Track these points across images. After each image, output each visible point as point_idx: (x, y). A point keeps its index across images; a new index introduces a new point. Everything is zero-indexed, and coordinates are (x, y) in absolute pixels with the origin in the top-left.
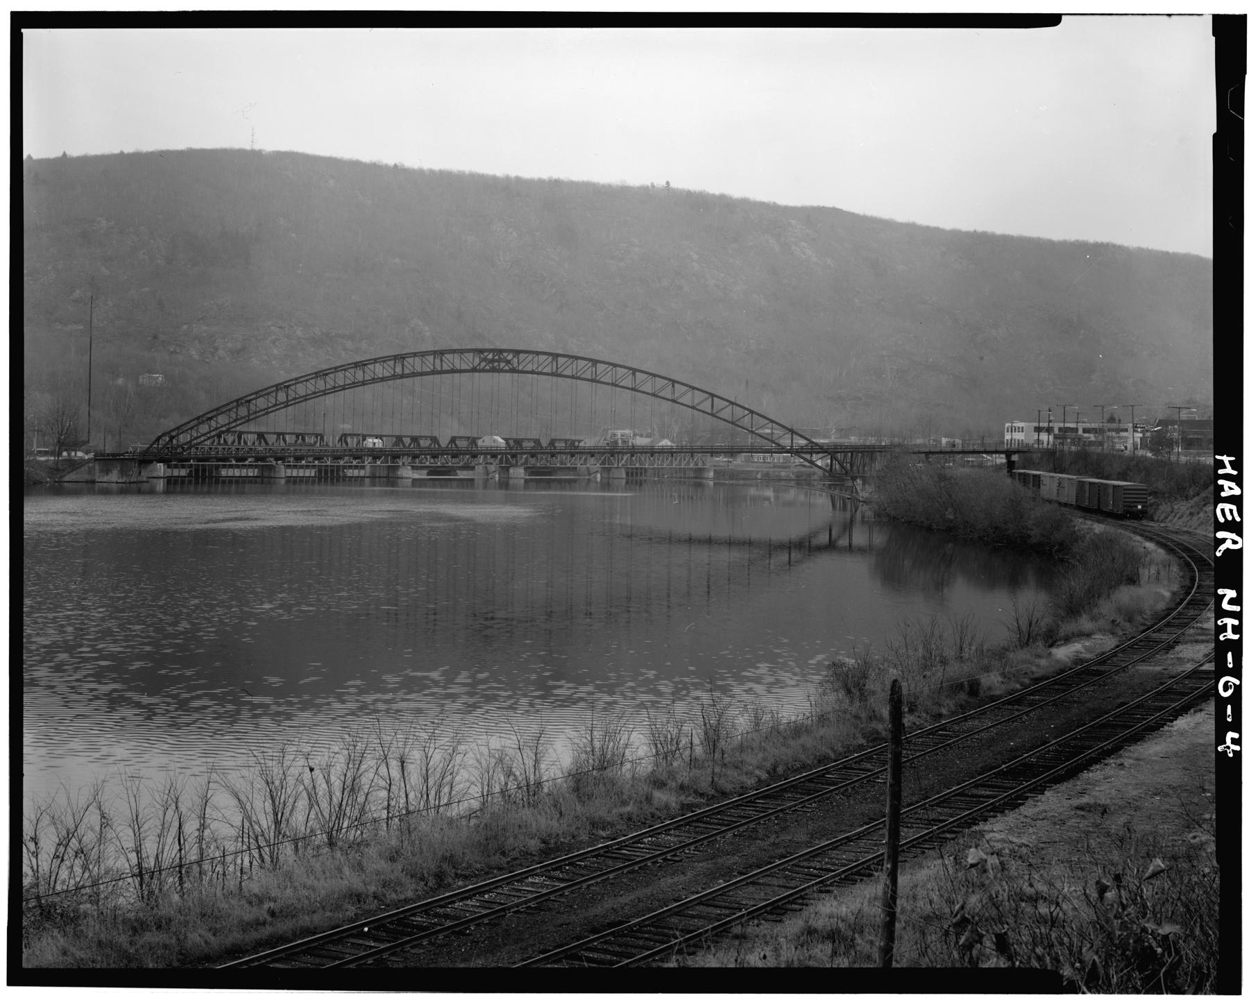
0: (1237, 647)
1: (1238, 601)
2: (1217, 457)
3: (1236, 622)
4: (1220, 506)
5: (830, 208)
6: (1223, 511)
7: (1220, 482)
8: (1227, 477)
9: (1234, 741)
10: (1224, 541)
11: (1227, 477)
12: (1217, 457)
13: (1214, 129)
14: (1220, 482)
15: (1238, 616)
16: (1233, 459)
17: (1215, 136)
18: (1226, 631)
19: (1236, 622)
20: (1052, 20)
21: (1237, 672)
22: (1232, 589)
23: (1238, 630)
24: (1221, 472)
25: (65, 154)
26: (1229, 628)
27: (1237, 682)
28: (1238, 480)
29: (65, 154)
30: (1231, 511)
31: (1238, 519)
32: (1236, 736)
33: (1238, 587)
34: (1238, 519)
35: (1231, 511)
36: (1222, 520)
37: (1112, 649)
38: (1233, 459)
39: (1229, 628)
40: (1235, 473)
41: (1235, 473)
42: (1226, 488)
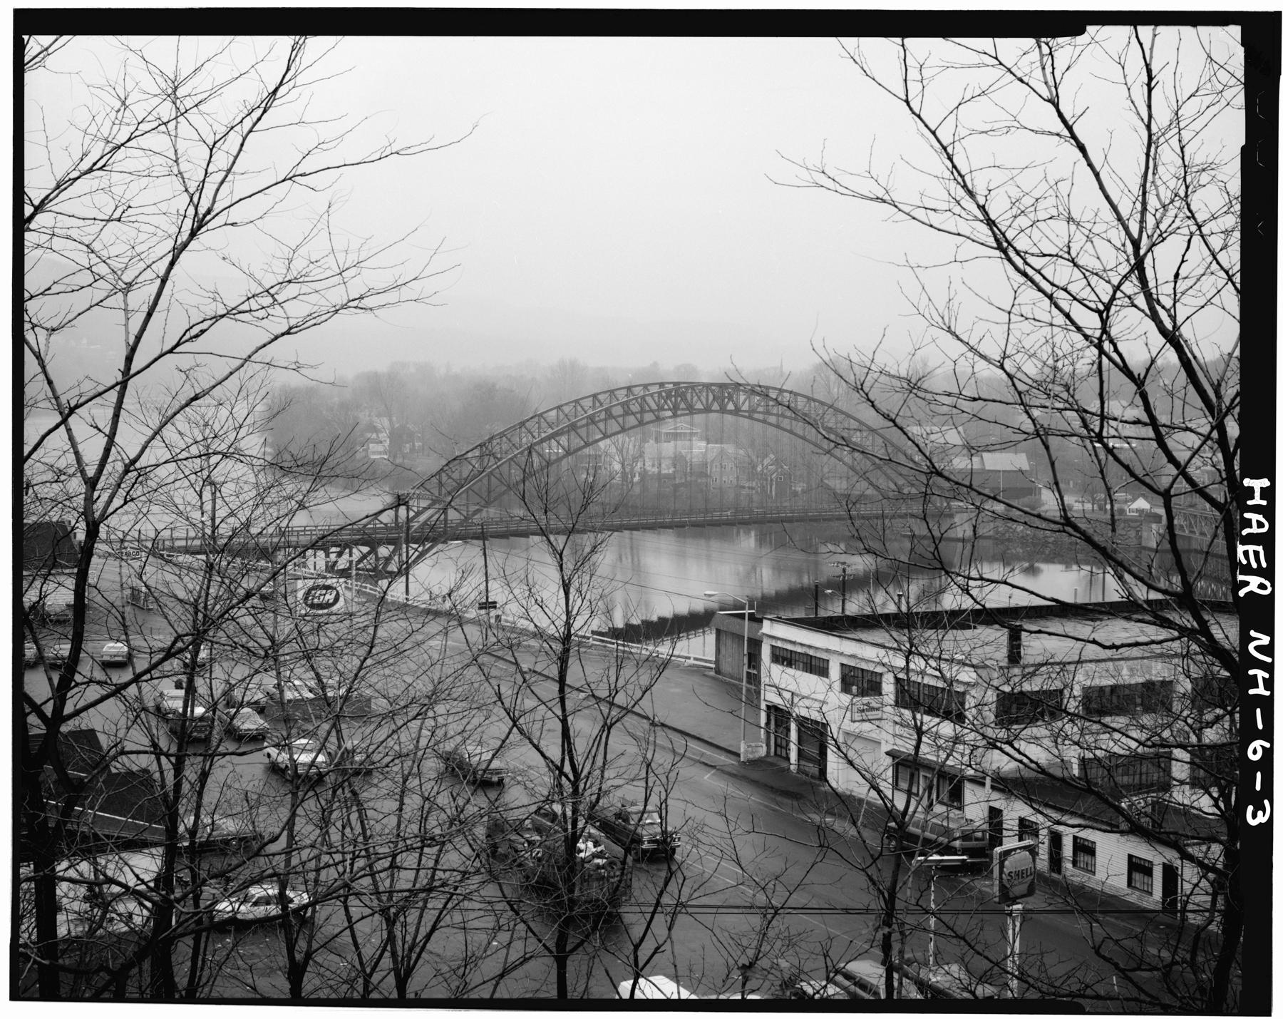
0: (1267, 705)
3: (1265, 483)
6: (1246, 553)
7: (1247, 515)
8: (1256, 509)
10: (1246, 584)
11: (1256, 509)
13: (1242, 141)
14: (1247, 515)
15: (1269, 668)
16: (1252, 692)
17: (1243, 148)
21: (1268, 734)
23: (1269, 684)
24: (1250, 503)
25: (655, 364)
26: (1257, 494)
27: (1267, 745)
29: (655, 364)
30: (1256, 554)
31: (1264, 565)
32: (1265, 640)
33: (1270, 631)
35: (1256, 554)
36: (1254, 565)
37: (1093, 828)
38: (1252, 692)
39: (1257, 494)
40: (1264, 503)
41: (1264, 503)
42: (1254, 524)
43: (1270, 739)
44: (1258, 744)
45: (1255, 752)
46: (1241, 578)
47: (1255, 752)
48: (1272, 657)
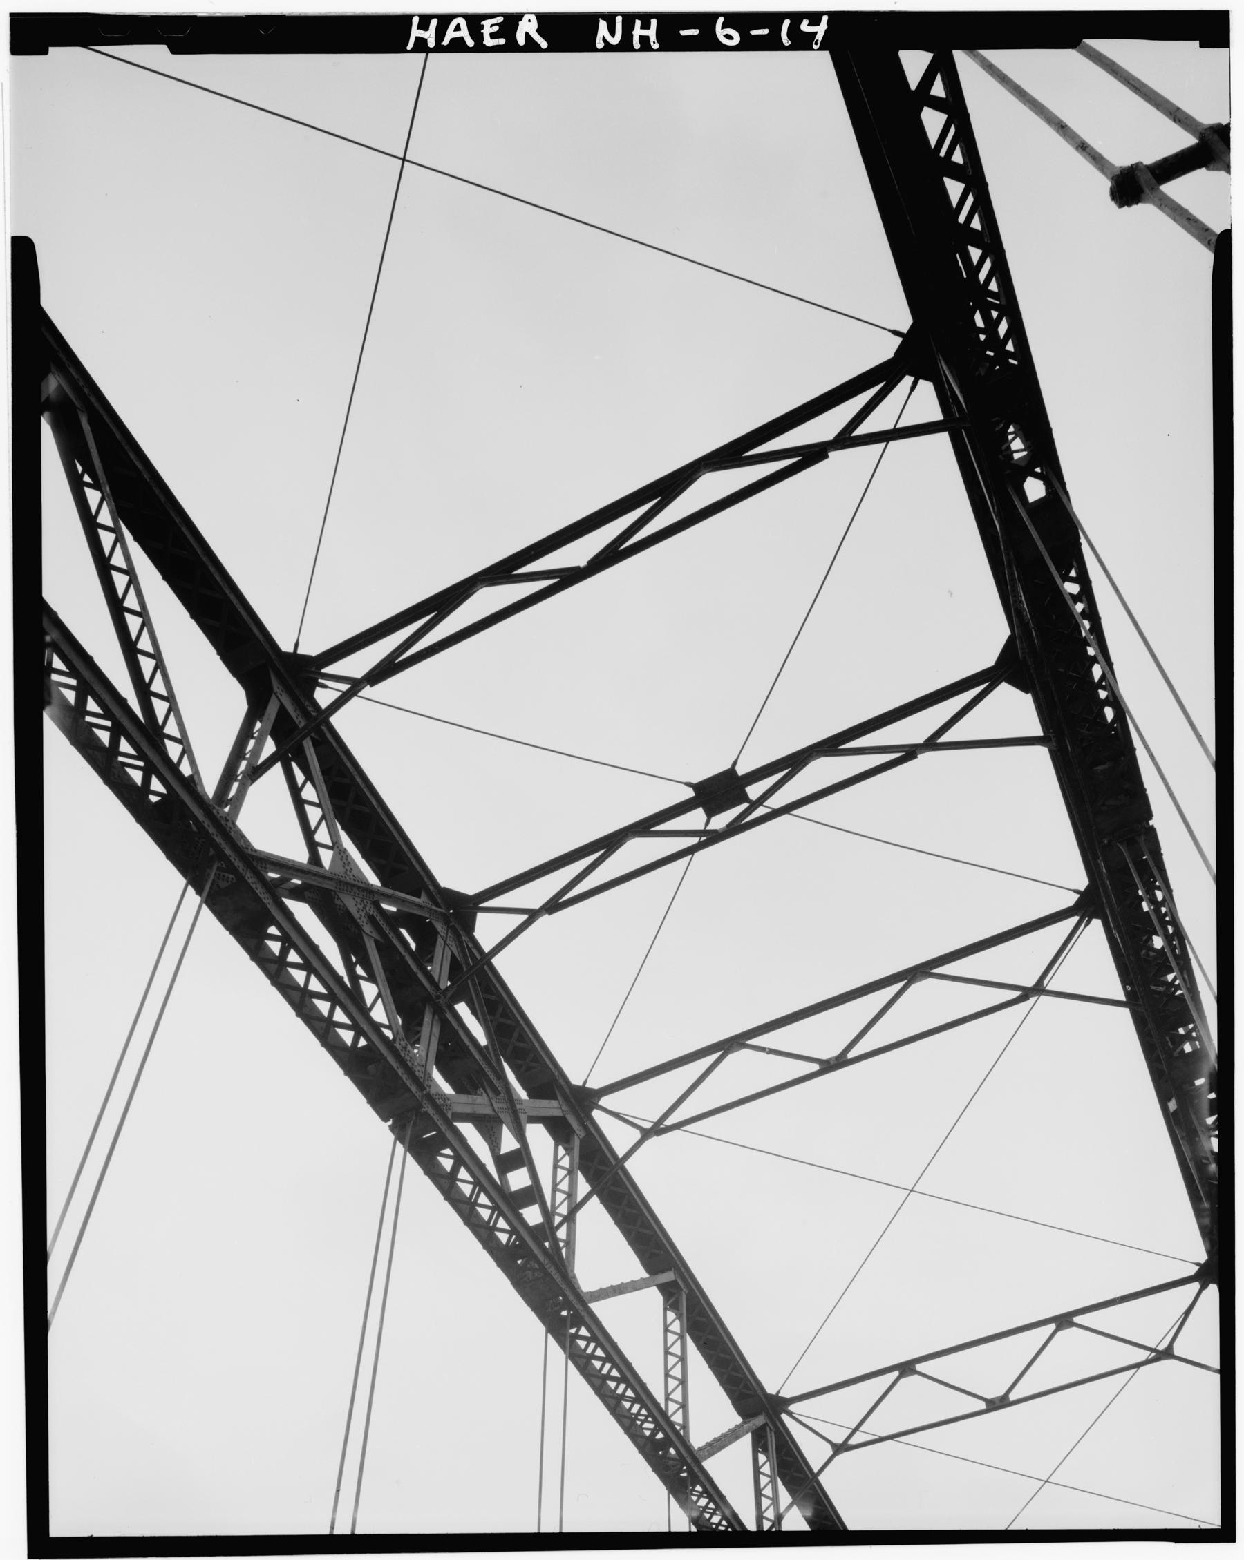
1: (610, 18)
2: (410, 47)
3: (638, 23)
4: (488, 42)
5: (599, 1290)
9: (644, 41)
10: (527, 36)
12: (410, 47)
15: (629, 19)
18: (648, 37)
19: (638, 23)
20: (23, 250)
22: (802, 21)
23: (645, 18)
26: (645, 33)
27: (721, 20)
28: (444, 20)
32: (603, 26)
34: (500, 19)
39: (645, 33)
42: (458, 34)
43: (714, 16)
44: (720, 33)
45: (729, 37)
46: (521, 40)
47: (729, 37)
48: (822, 14)
